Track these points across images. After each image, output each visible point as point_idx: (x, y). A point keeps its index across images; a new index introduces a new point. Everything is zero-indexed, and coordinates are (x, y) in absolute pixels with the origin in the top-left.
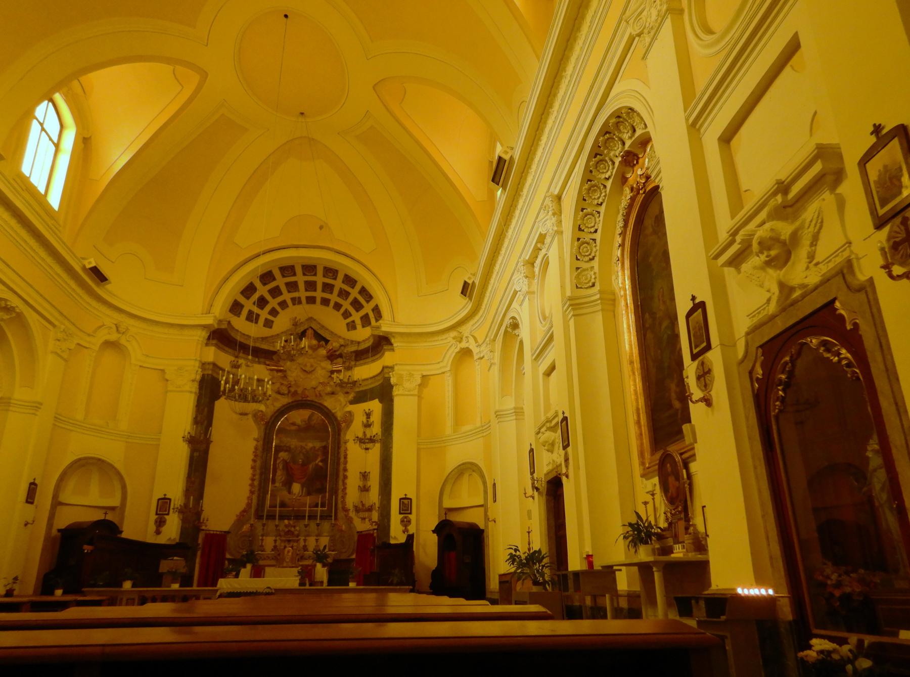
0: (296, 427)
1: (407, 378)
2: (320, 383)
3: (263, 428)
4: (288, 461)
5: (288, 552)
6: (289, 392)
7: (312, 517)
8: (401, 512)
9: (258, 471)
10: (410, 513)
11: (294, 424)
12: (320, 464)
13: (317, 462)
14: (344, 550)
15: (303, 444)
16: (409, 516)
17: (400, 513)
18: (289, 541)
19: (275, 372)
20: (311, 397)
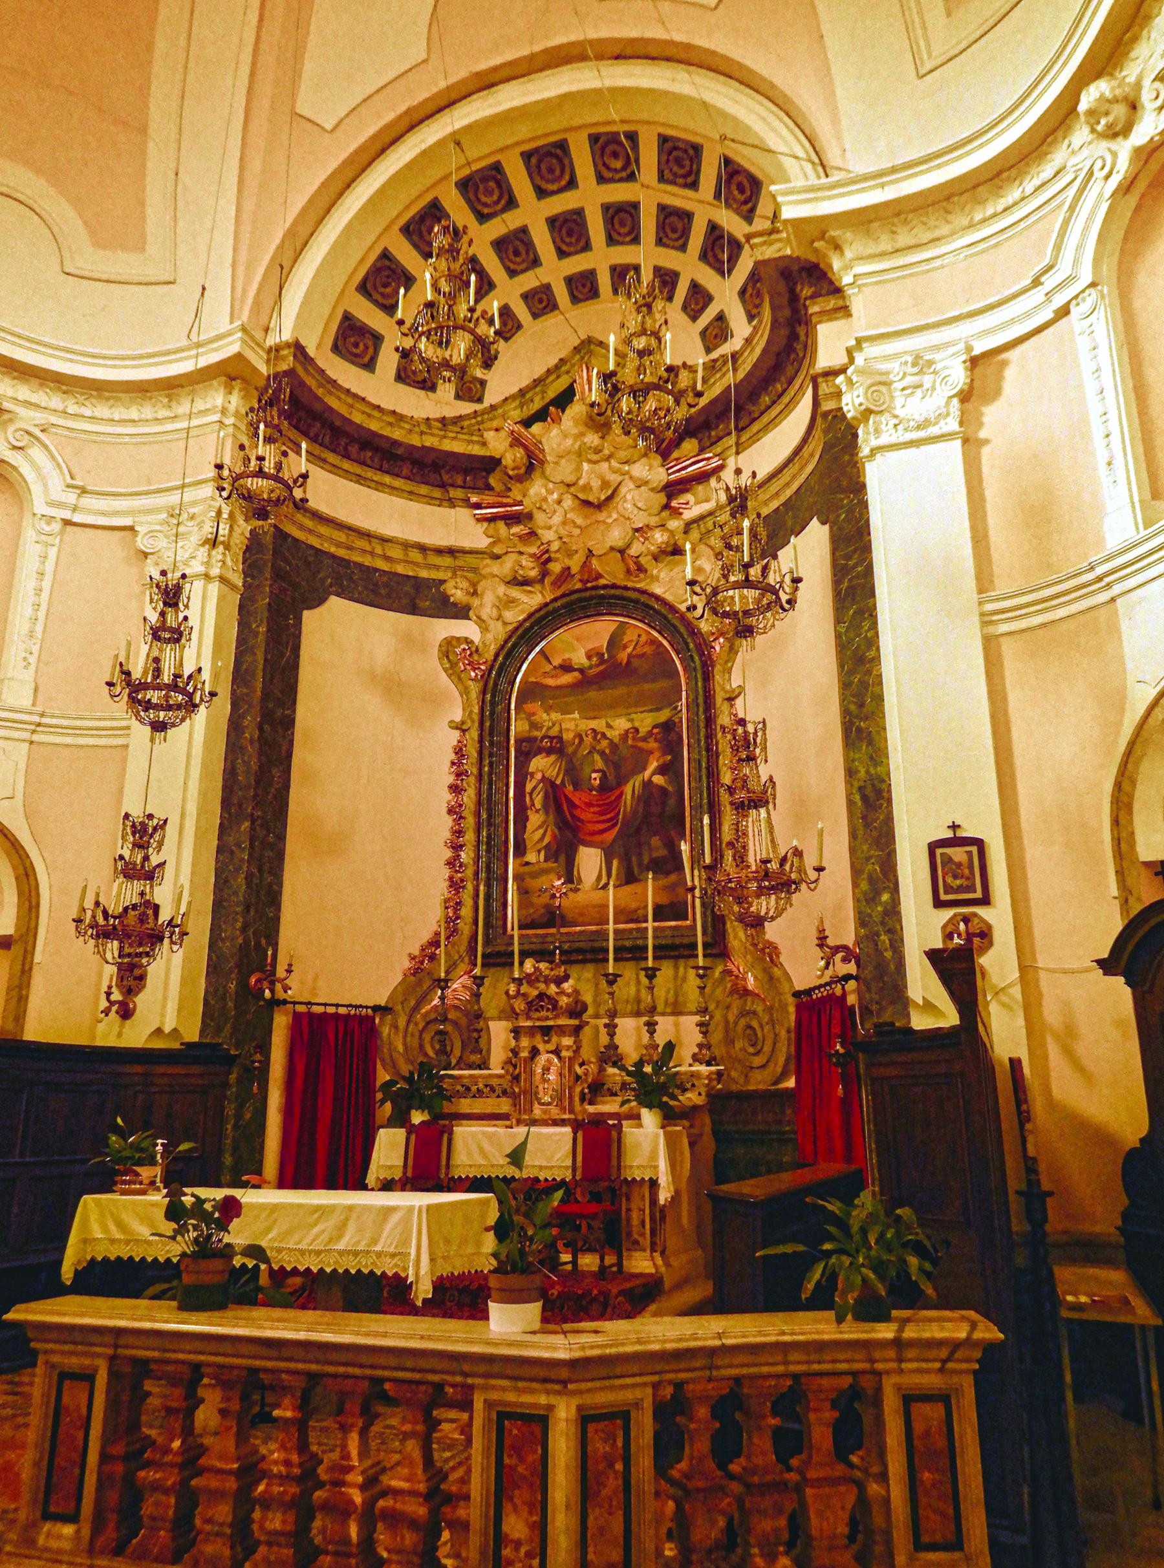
0: (576, 674)
1: (909, 380)
2: (637, 530)
3: (474, 689)
4: (558, 782)
5: (546, 1070)
6: (544, 574)
7: (631, 952)
8: (943, 897)
9: (470, 821)
10: (985, 901)
11: (566, 668)
12: (658, 780)
13: (647, 774)
14: (758, 1061)
15: (599, 724)
16: (981, 911)
17: (938, 904)
18: (546, 1031)
19: (501, 524)
20: (611, 572)
